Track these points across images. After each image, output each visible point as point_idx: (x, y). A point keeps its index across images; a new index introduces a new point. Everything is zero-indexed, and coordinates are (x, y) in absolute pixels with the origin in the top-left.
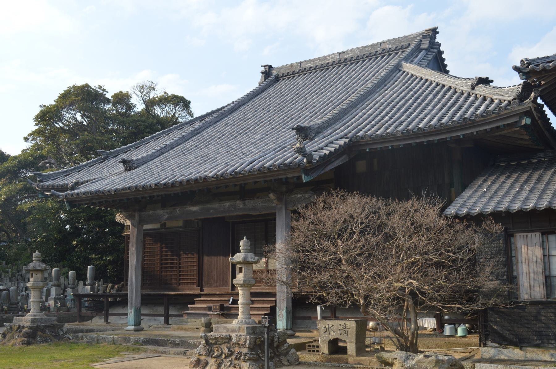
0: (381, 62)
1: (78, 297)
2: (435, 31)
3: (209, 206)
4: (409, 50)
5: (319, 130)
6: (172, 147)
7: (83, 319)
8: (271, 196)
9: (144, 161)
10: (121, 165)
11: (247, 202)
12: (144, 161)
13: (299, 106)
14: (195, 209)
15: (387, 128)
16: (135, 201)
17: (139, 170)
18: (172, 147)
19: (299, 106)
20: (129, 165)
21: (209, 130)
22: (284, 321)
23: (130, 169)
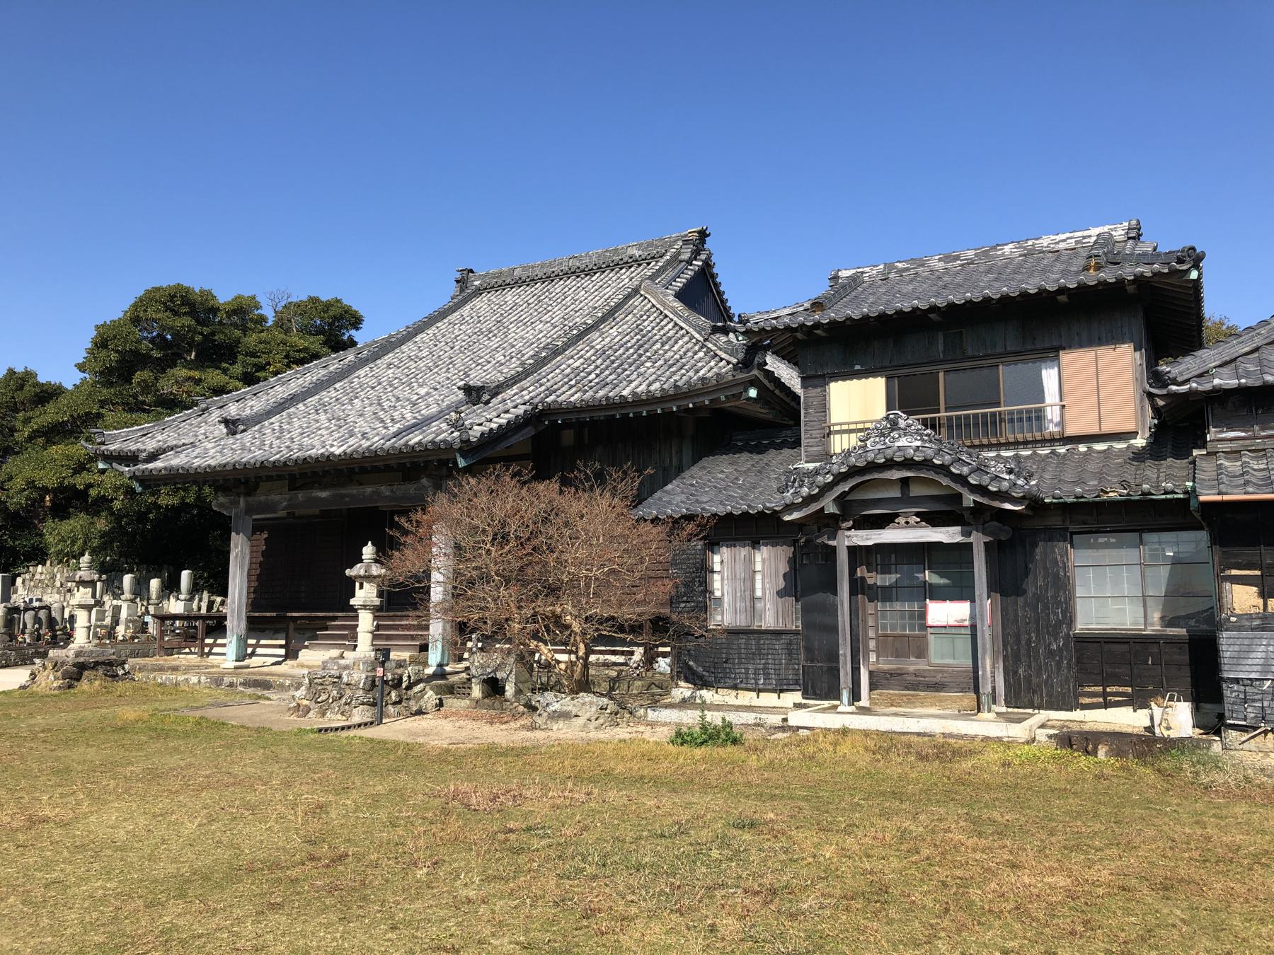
0: (625, 274)
1: (162, 618)
2: (703, 235)
3: (343, 491)
4: (656, 266)
5: (497, 390)
6: (294, 399)
7: (170, 651)
8: (424, 481)
9: (258, 419)
10: (222, 426)
11: (395, 488)
12: (258, 419)
13: (494, 343)
14: (324, 494)
15: (650, 385)
16: (241, 481)
17: (247, 438)
18: (294, 399)
19: (494, 343)
20: (232, 425)
21: (362, 372)
22: (439, 654)
23: (234, 433)
